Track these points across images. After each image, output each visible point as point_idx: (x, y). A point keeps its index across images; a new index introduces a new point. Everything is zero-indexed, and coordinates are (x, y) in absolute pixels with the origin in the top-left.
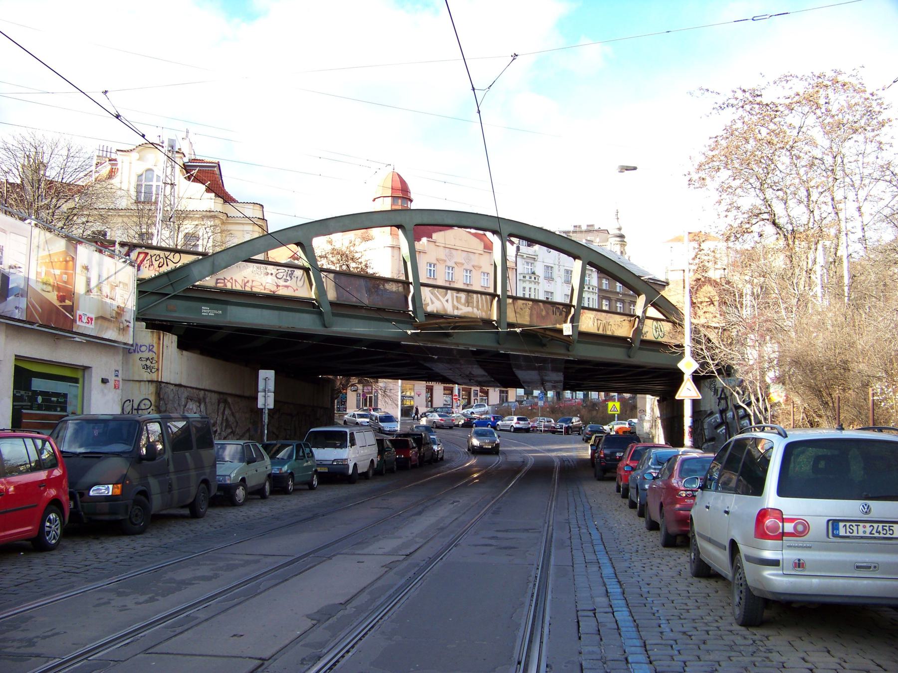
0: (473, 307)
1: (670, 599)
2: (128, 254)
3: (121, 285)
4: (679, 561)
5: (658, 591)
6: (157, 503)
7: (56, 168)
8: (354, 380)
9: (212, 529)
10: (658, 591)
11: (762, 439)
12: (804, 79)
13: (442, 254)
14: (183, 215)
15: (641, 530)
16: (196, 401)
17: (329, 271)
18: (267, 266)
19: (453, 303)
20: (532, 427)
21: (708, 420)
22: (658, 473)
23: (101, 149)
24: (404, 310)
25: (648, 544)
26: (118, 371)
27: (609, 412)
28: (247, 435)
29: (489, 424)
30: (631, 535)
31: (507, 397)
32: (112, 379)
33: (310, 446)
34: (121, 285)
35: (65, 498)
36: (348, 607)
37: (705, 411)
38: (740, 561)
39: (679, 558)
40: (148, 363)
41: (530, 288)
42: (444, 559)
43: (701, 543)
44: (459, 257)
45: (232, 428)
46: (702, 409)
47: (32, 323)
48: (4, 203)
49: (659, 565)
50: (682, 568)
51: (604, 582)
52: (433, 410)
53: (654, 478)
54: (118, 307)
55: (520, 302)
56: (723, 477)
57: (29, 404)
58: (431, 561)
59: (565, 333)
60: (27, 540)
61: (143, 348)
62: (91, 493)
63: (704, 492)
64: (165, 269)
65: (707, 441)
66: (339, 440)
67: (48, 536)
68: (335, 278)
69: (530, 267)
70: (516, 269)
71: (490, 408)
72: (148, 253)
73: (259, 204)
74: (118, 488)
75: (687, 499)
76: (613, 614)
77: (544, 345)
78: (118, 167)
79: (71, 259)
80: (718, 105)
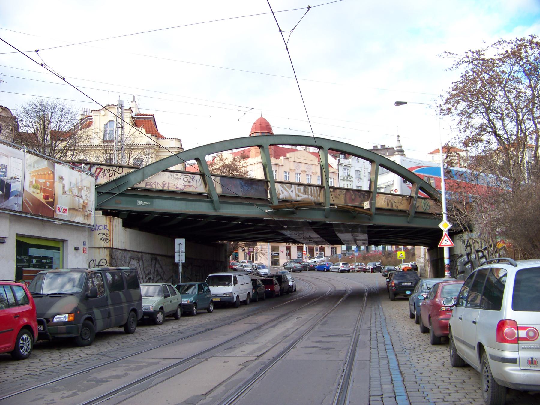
0: (308, 195)
1: (436, 384)
2: (90, 169)
3: (85, 189)
4: (443, 355)
5: (428, 379)
6: (99, 325)
7: (55, 122)
8: (242, 243)
9: (137, 341)
10: (428, 379)
11: (500, 269)
12: (511, 43)
13: (292, 166)
14: (131, 148)
15: (417, 333)
16: (136, 260)
17: (217, 176)
18: (177, 173)
19: (296, 193)
20: (351, 269)
21: (459, 260)
22: (427, 295)
23: (83, 110)
24: (266, 198)
25: (422, 343)
26: (85, 242)
27: (399, 258)
28: (171, 280)
29: (325, 268)
30: (410, 337)
31: (336, 251)
32: (81, 247)
33: (208, 285)
34: (85, 189)
35: (34, 324)
36: (207, 397)
37: (457, 254)
38: (486, 358)
39: (443, 353)
40: (104, 236)
41: (347, 185)
42: (283, 358)
43: (457, 344)
44: (303, 167)
45: (161, 275)
46: (456, 253)
47: (26, 213)
48: (13, 141)
49: (429, 358)
50: (445, 360)
51: (390, 372)
52: (291, 261)
53: (425, 299)
54: (83, 202)
55: (338, 190)
56: (471, 297)
57: (28, 264)
58: (275, 359)
59: (365, 208)
60: (8, 353)
61: (101, 228)
62: (55, 320)
63: (458, 307)
64: (113, 178)
65: (459, 273)
66: (225, 281)
67: (22, 349)
68: (220, 180)
69: (347, 172)
70: (338, 173)
71: (326, 258)
72: (102, 168)
73: (179, 139)
74: (72, 316)
75: (447, 312)
76: (395, 398)
77: (354, 217)
78: (93, 120)
79: (52, 173)
80: (457, 62)
